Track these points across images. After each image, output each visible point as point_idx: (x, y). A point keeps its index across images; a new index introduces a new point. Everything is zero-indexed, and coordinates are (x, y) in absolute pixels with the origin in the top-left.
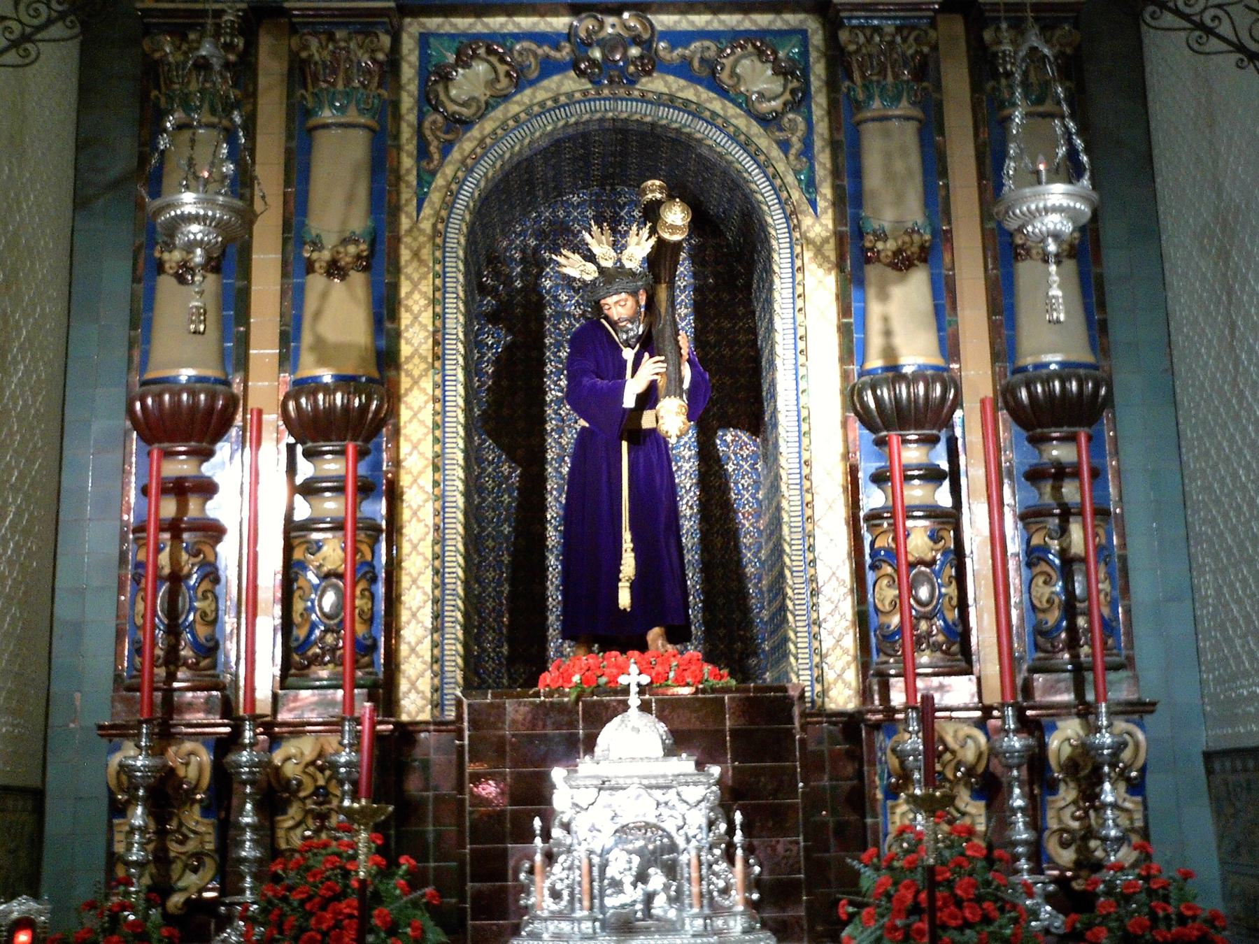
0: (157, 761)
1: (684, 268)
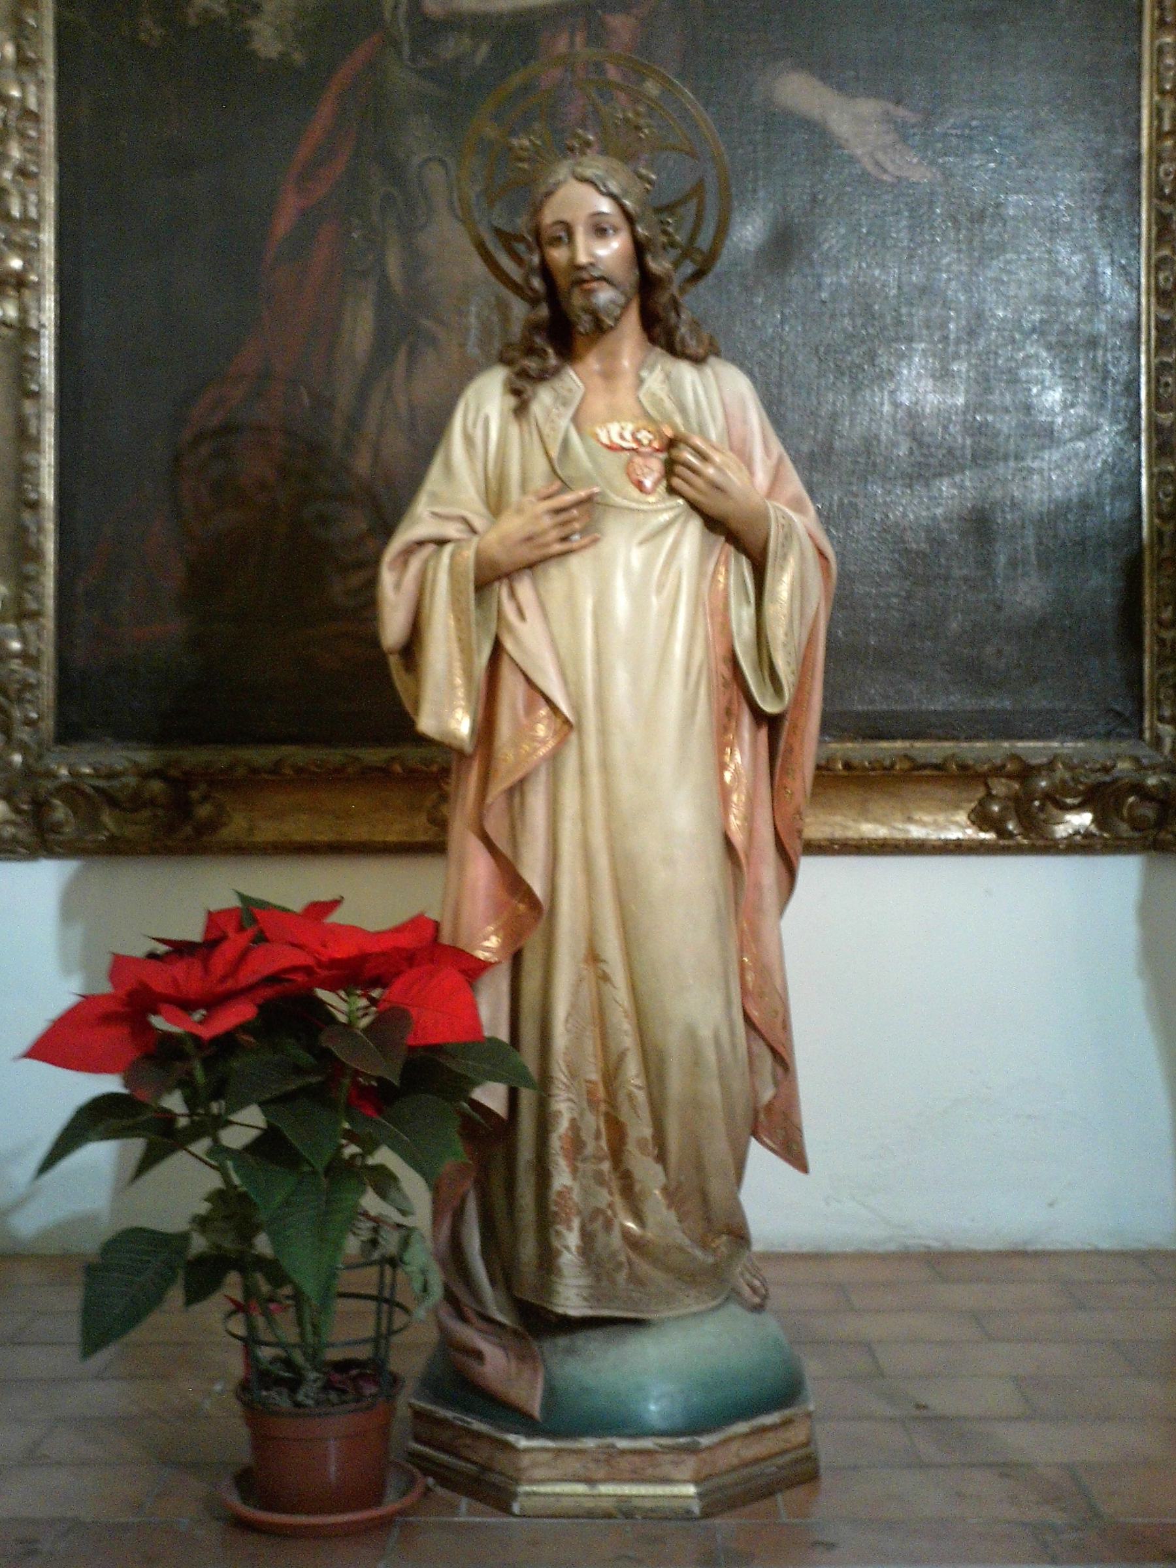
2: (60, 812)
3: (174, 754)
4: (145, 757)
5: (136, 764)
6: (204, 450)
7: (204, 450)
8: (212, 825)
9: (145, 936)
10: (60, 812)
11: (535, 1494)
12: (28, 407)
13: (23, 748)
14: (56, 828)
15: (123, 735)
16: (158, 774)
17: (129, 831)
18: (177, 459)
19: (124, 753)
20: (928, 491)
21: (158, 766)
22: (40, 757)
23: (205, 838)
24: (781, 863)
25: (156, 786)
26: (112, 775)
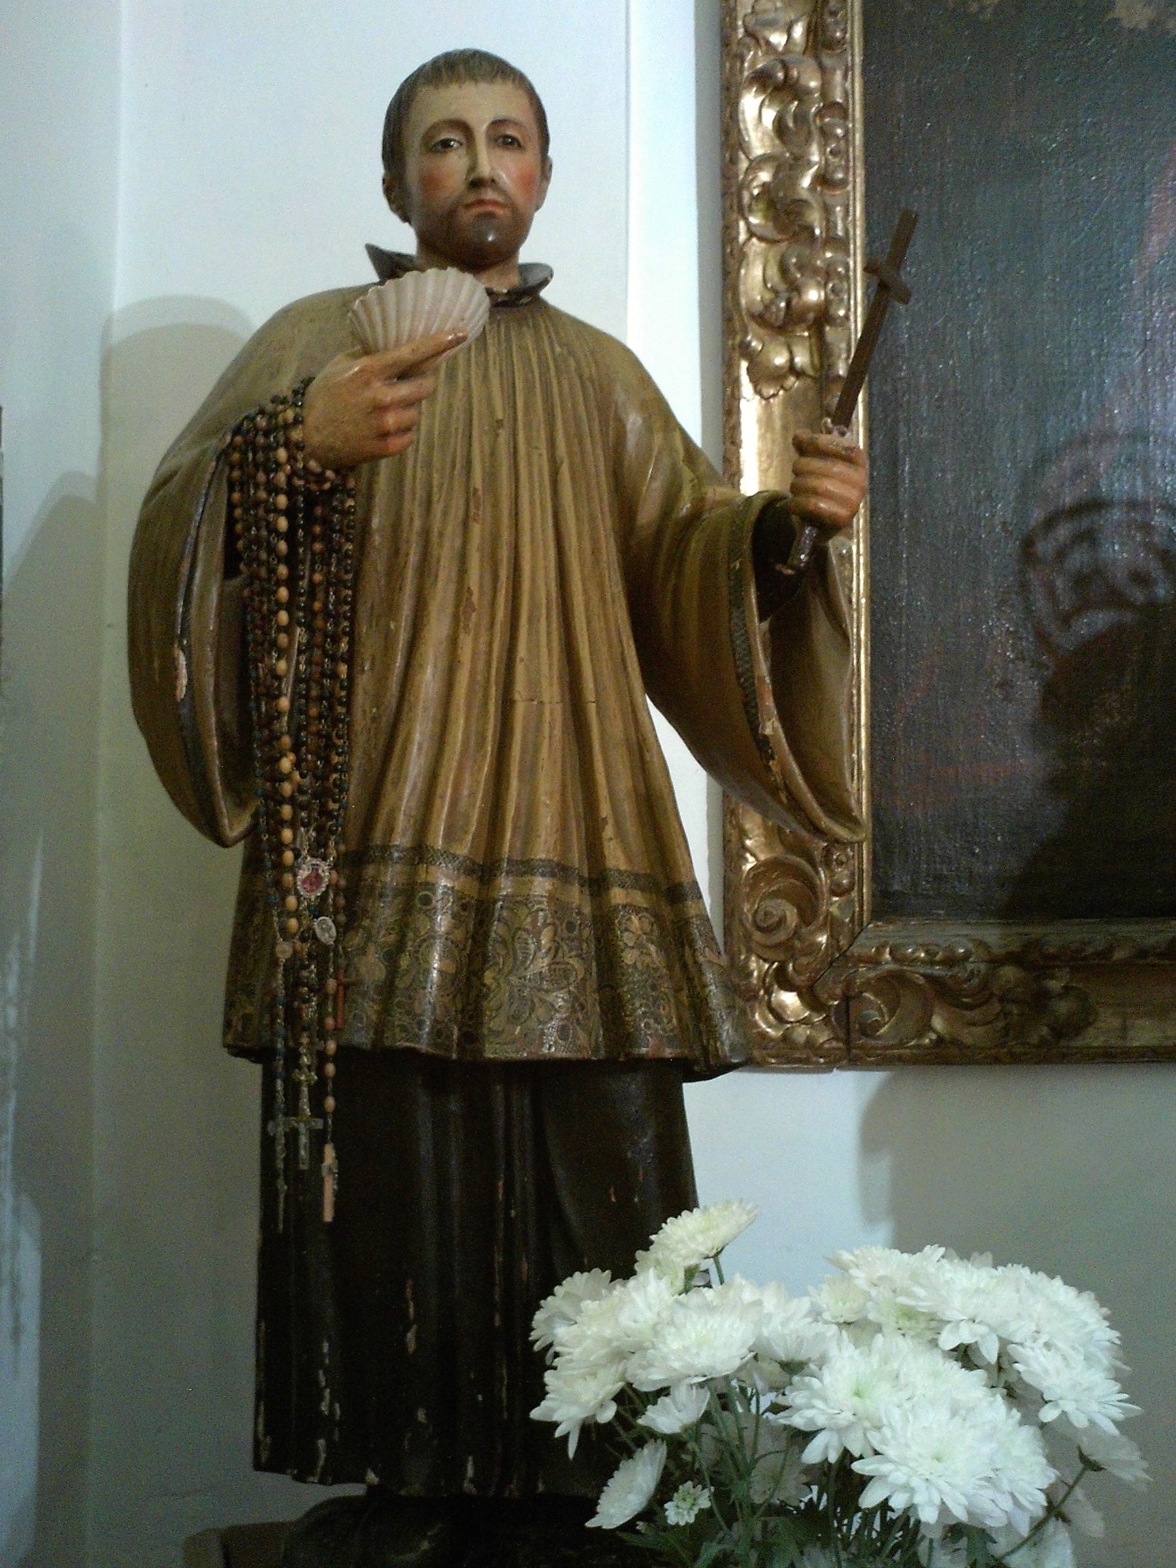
0: (262, 488)
2: (873, 1007)
3: (1036, 931)
4: (993, 935)
5: (981, 944)
6: (1063, 532)
7: (1063, 532)
8: (1064, 1030)
9: (828, 1259)
10: (873, 1007)
12: (517, 856)
13: (831, 924)
14: (869, 1030)
15: (960, 909)
16: (1012, 958)
17: (973, 1036)
18: (1028, 544)
19: (965, 931)
20: (625, 1371)
21: (1015, 947)
22: (854, 938)
23: (1063, 1043)
24: (570, 723)
25: (1009, 973)
26: (951, 961)
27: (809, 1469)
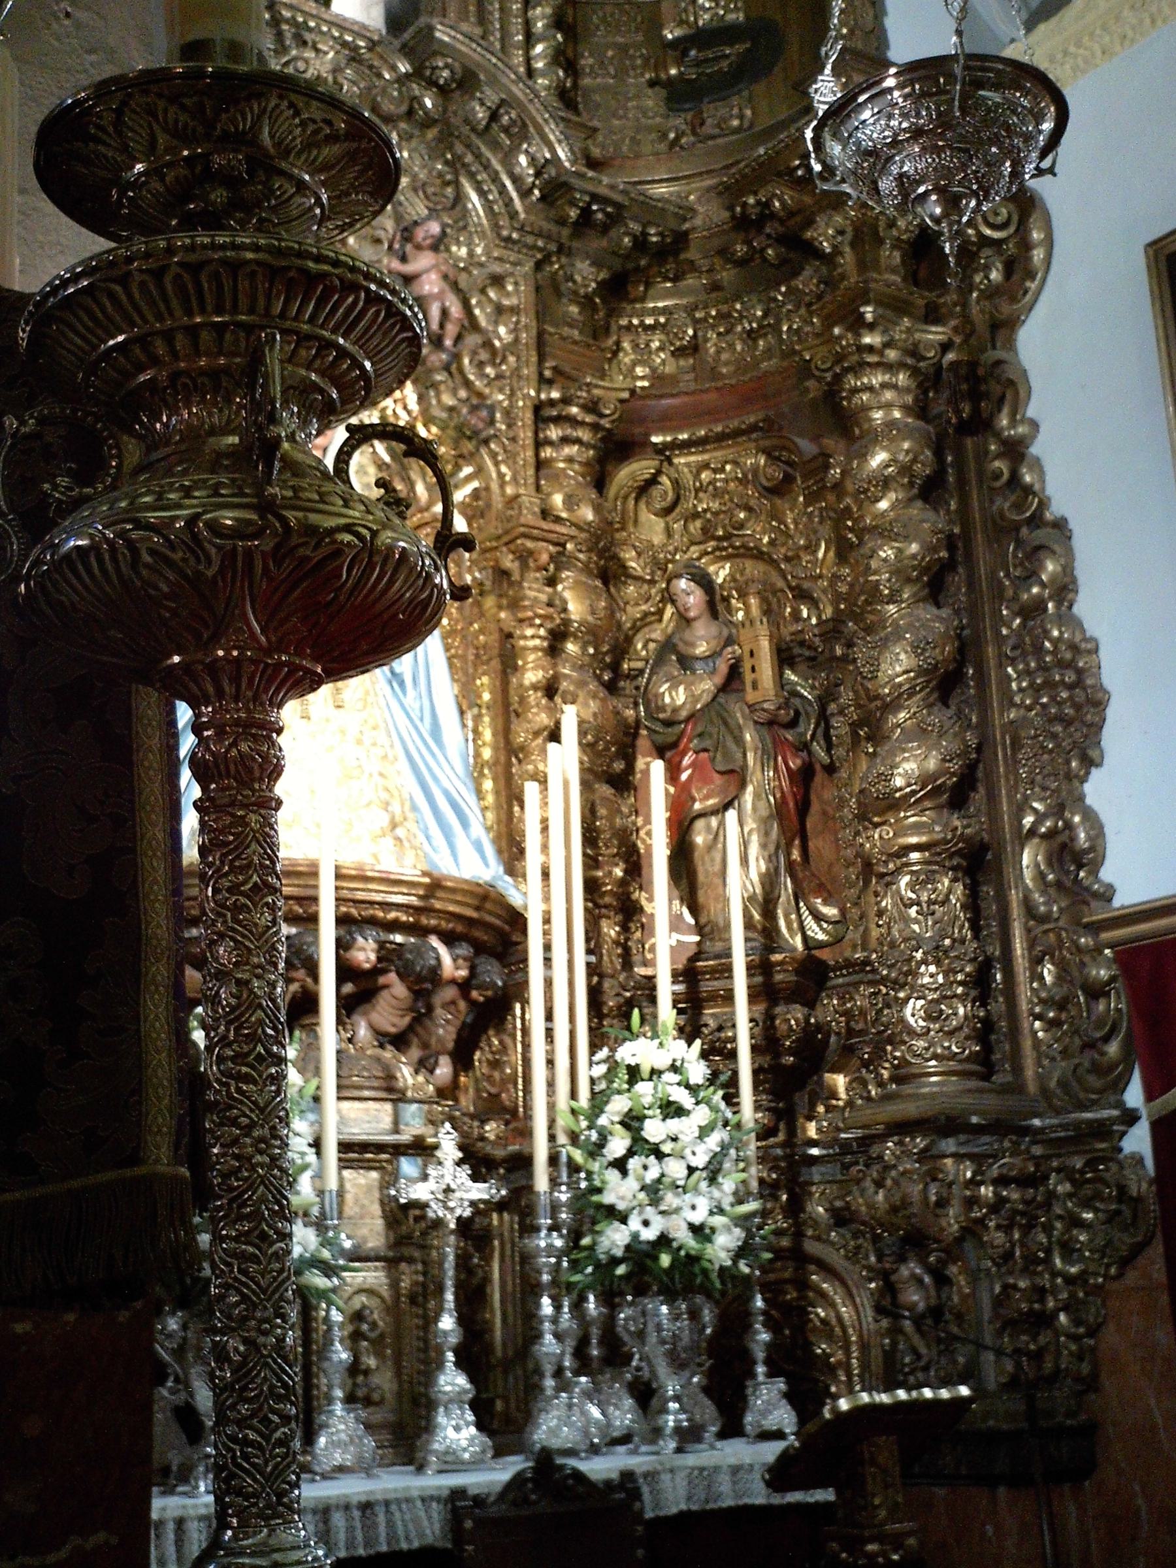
1: (354, 420)
11: (298, 886)
27: (1054, 984)
